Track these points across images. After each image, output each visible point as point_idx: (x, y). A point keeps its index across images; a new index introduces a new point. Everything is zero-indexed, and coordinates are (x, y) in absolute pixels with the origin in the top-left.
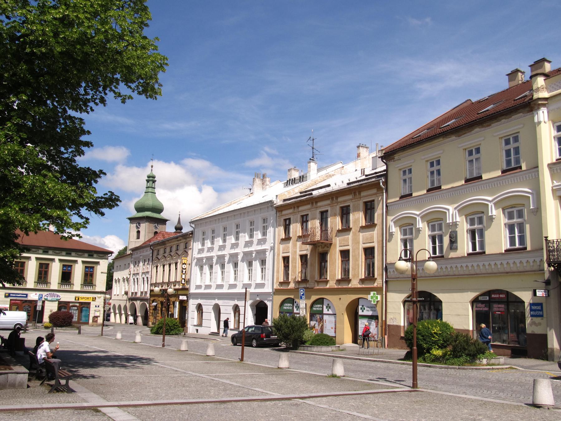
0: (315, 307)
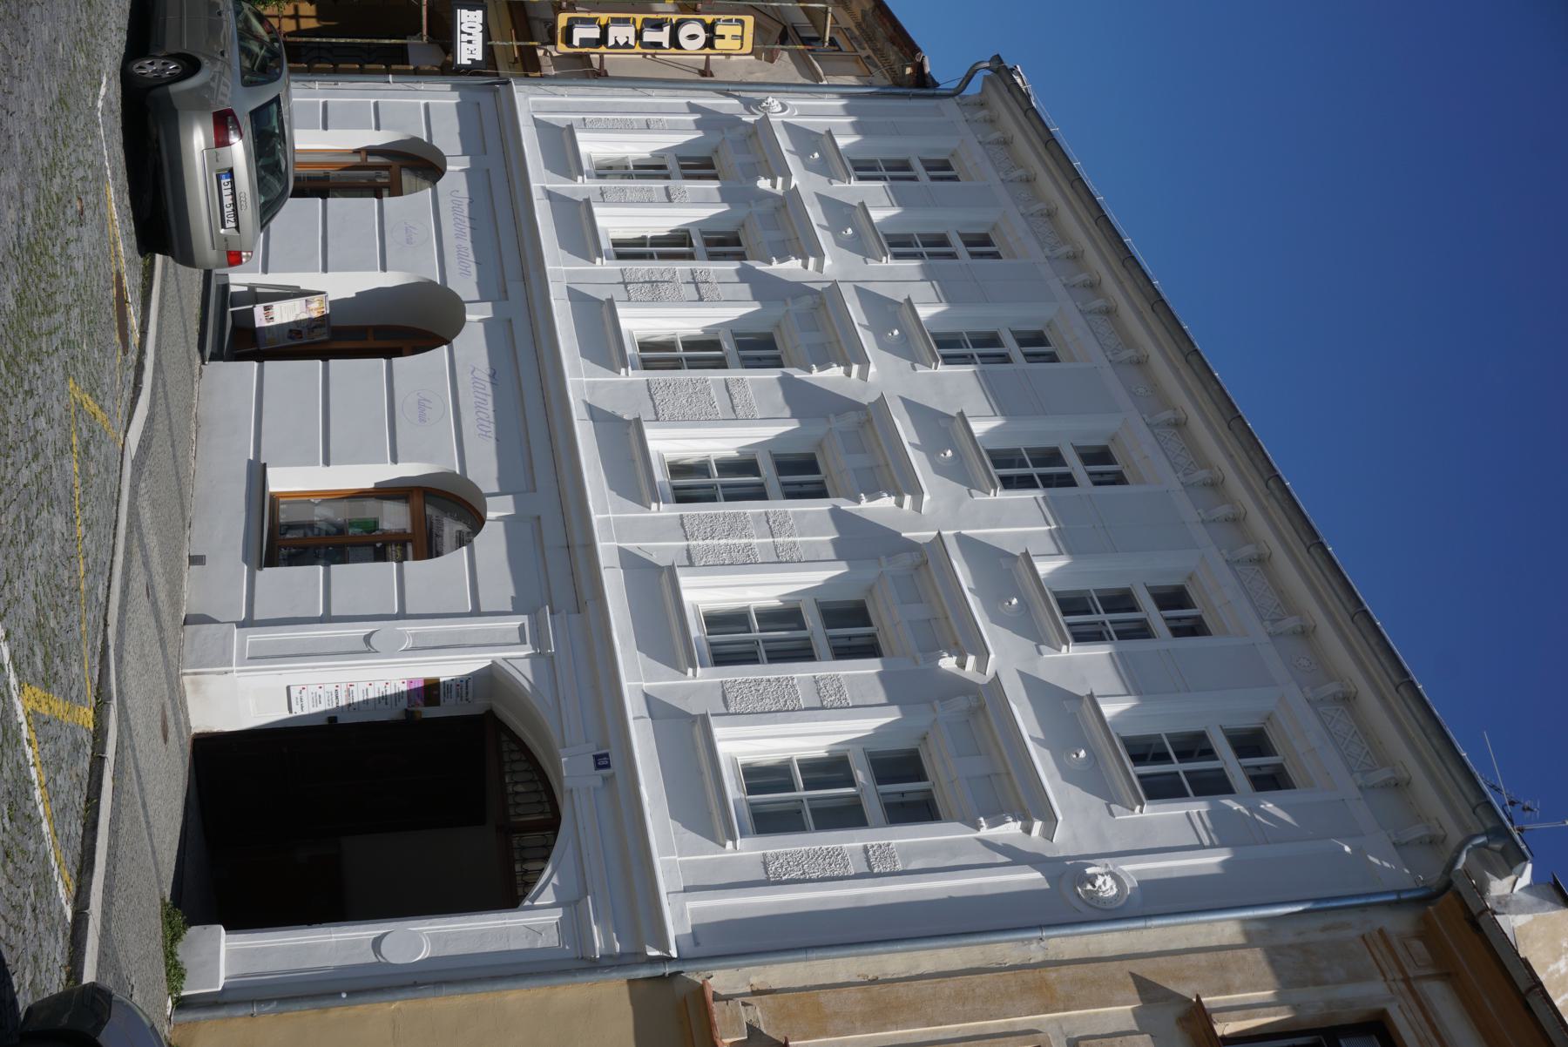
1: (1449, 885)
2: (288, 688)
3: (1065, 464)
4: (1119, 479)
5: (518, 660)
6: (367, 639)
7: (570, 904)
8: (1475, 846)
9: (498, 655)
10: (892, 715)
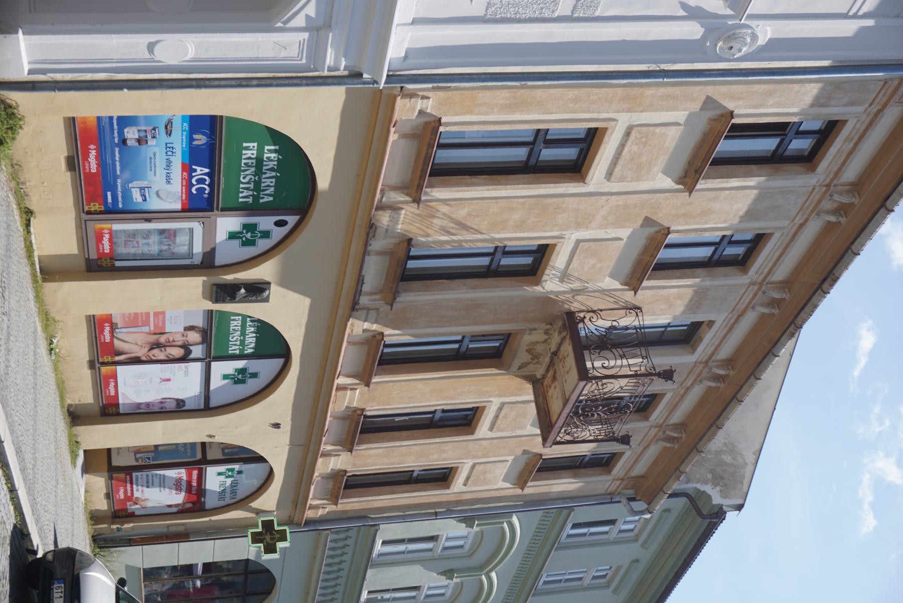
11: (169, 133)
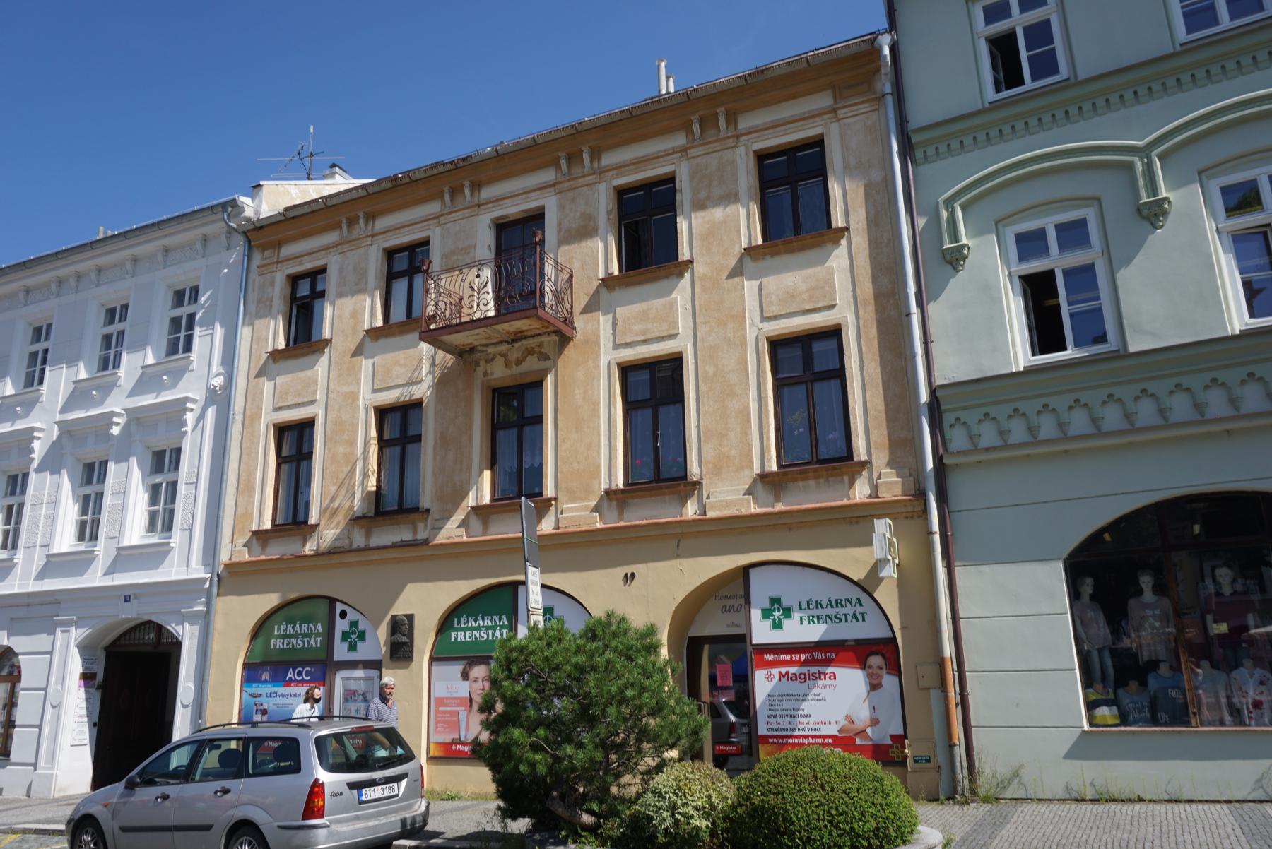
0: (465, 630)
1: (244, 233)
2: (72, 746)
3: (182, 317)
4: (125, 307)
5: (77, 634)
6: (53, 707)
7: (183, 618)
8: (228, 218)
9: (73, 643)
10: (134, 461)
11: (260, 695)
